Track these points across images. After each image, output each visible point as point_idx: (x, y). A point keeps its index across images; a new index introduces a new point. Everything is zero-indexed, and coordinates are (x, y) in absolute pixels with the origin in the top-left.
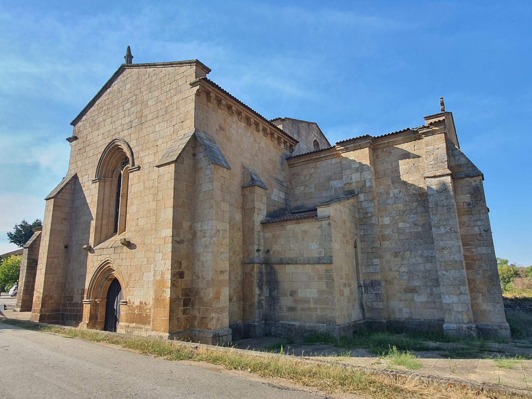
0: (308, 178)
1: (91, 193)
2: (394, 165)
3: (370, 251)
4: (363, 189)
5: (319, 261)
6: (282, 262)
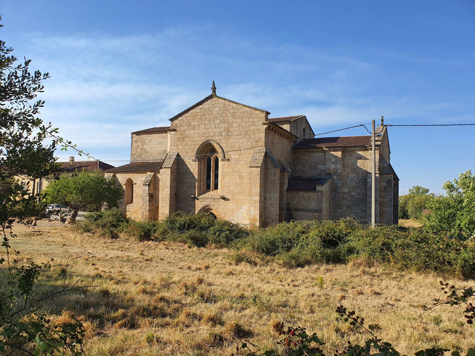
0: (304, 161)
1: (193, 167)
2: (353, 162)
3: (336, 205)
4: (336, 173)
5: (316, 211)
6: (296, 210)
